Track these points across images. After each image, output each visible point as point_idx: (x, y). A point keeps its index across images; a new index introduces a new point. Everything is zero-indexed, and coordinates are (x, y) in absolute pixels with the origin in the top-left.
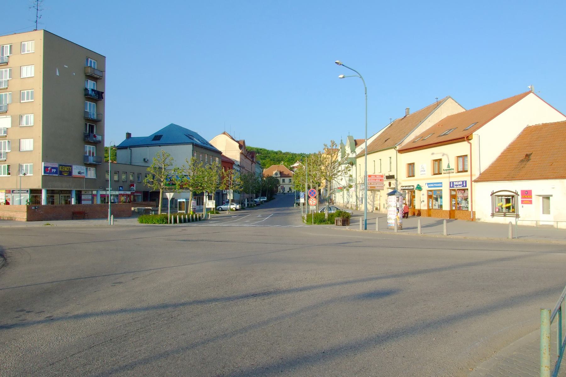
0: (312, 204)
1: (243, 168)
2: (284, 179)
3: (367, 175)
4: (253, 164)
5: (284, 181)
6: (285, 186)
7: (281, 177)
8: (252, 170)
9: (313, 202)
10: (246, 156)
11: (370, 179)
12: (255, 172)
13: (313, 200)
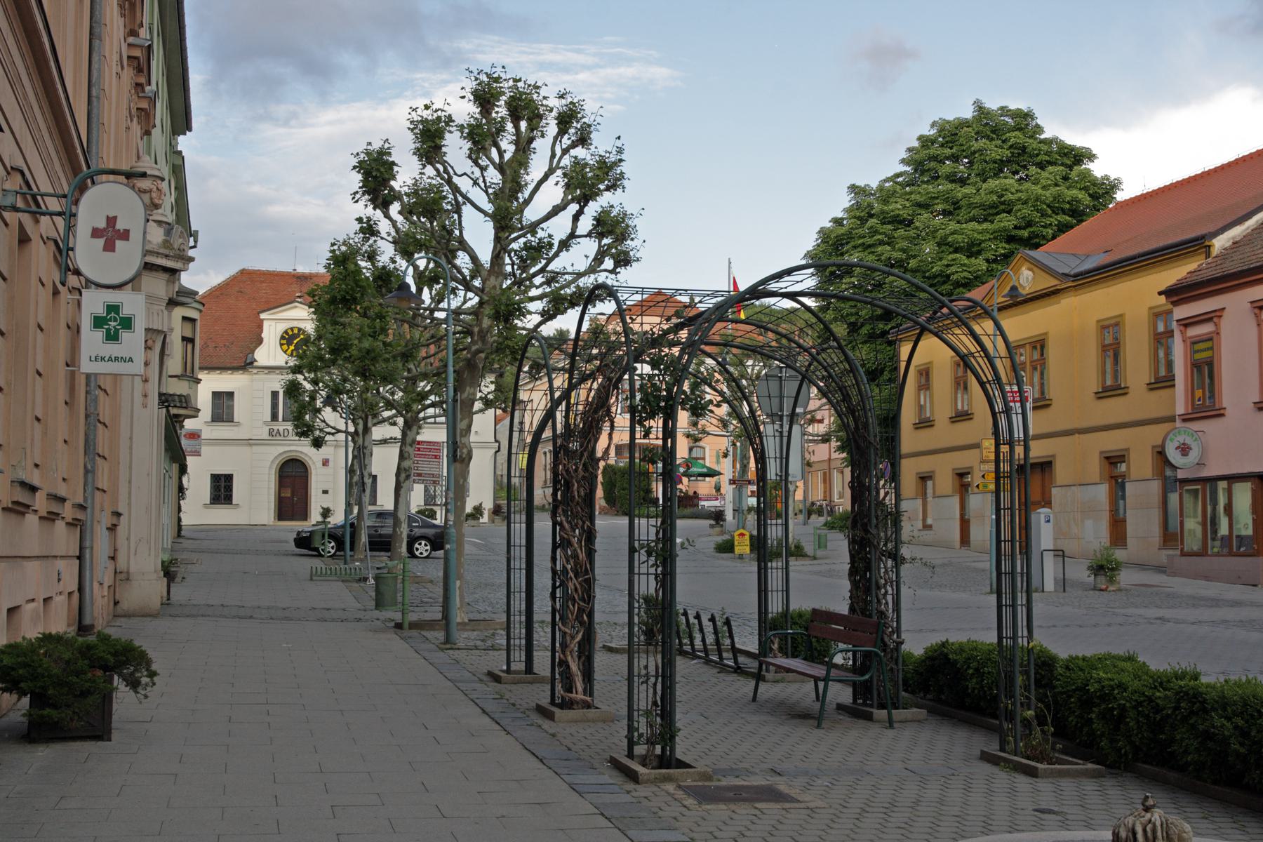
2: (230, 395)
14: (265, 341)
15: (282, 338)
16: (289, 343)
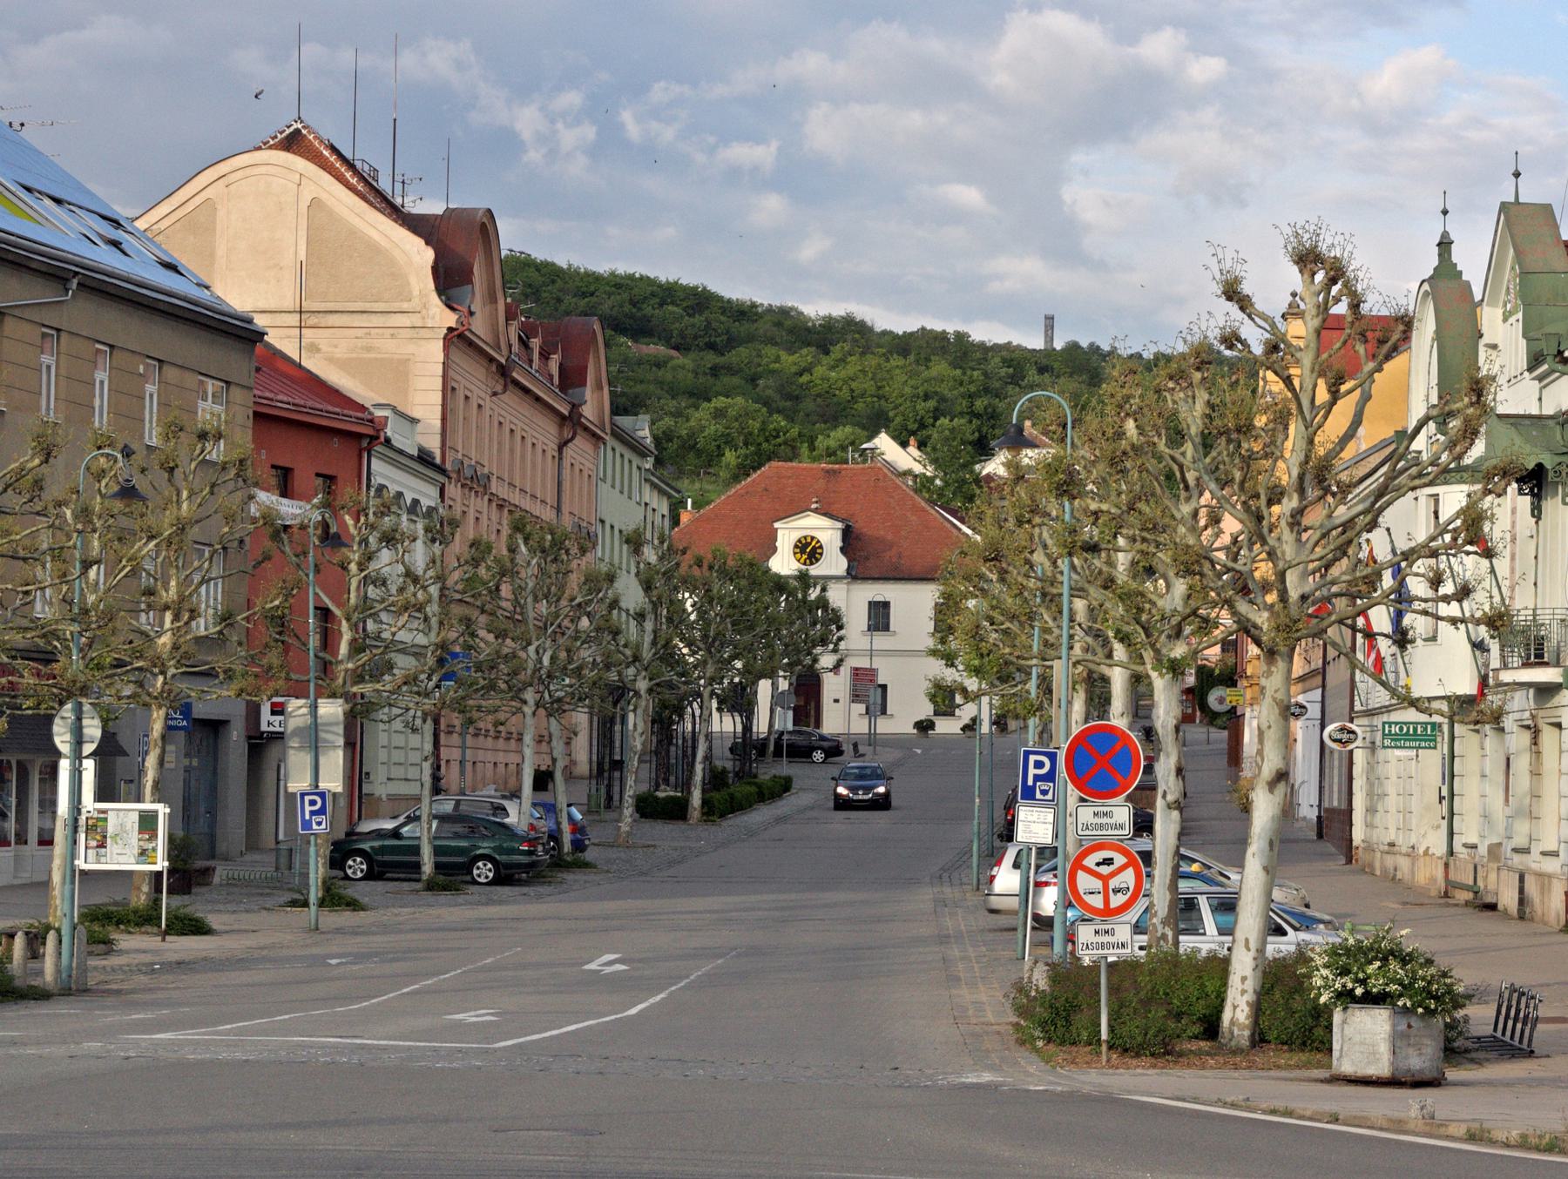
0: (1097, 901)
1: (476, 482)
2: (886, 605)
4: (569, 451)
5: (879, 615)
7: (855, 574)
9: (1113, 883)
10: (503, 371)
14: (779, 550)
15: (796, 546)
16: (803, 552)
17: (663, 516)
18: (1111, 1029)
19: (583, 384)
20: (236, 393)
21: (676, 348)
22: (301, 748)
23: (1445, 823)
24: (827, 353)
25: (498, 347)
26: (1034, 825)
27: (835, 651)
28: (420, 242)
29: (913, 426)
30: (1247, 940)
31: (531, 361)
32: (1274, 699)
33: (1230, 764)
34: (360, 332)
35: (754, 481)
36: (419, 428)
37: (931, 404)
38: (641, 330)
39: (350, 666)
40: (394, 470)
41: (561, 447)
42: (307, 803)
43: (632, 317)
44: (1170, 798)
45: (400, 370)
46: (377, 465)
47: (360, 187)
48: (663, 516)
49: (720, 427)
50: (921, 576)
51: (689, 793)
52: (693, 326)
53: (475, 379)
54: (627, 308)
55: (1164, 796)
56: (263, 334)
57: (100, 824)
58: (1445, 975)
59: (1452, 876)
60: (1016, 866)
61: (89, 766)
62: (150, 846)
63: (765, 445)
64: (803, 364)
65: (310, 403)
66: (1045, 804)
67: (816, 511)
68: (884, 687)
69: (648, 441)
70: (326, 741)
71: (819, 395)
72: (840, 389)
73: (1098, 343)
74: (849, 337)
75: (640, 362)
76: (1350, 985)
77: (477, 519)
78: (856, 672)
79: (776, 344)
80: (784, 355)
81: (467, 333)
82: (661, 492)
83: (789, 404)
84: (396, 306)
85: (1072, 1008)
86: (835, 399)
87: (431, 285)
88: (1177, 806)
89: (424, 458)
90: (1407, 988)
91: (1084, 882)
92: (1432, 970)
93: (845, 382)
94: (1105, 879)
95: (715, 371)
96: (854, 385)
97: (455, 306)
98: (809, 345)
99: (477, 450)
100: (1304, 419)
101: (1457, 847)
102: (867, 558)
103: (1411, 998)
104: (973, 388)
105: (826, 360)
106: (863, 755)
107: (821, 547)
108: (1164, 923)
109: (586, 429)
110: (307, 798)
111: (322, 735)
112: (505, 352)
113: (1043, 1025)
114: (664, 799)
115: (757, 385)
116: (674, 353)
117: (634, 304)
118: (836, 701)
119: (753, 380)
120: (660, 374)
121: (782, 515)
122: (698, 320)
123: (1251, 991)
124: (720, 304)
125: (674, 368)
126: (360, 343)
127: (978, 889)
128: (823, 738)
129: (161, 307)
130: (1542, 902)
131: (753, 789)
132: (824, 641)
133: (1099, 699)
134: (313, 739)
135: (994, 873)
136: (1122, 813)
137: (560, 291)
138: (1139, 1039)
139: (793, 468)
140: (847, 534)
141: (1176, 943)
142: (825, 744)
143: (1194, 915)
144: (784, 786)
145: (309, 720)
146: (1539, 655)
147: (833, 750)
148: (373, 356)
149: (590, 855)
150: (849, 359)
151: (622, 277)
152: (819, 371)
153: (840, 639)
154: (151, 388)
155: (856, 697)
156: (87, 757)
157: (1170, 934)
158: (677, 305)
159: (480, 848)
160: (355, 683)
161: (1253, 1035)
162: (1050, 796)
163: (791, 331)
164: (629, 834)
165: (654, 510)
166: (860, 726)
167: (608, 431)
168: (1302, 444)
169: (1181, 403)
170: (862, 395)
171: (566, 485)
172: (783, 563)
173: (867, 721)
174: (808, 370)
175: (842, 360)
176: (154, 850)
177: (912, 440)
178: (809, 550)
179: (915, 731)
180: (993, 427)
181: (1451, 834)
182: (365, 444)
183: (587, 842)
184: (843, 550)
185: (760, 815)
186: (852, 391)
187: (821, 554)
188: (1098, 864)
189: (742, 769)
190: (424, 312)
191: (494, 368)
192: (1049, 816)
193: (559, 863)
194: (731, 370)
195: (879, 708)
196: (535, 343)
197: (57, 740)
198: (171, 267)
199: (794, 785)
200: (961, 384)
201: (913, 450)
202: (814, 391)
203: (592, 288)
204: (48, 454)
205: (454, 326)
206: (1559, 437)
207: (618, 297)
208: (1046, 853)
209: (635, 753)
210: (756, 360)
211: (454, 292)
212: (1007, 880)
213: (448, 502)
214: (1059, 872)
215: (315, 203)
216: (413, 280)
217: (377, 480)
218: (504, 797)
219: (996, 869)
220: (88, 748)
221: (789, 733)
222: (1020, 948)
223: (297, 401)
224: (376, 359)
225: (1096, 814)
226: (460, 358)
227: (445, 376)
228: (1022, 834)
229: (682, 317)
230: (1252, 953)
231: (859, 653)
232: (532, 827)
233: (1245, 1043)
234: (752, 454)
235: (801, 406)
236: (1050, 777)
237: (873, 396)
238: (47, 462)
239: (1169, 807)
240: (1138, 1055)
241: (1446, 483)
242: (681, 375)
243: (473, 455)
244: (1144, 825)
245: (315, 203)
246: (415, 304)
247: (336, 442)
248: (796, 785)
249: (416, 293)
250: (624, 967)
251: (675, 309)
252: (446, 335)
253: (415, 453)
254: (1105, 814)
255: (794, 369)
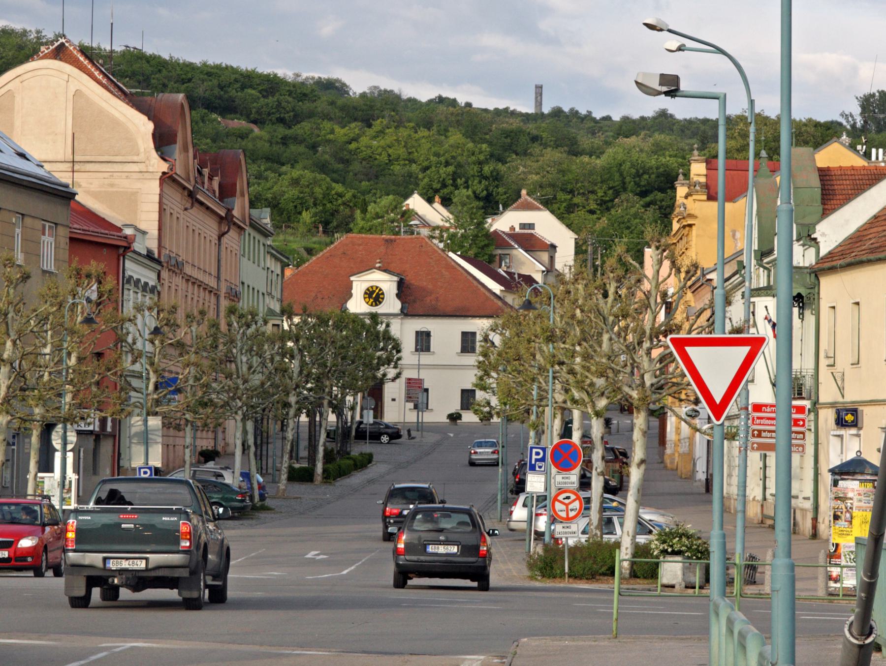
0: (564, 515)
1: (177, 267)
2: (428, 334)
3: (750, 402)
4: (225, 240)
5: (423, 341)
6: (429, 379)
7: (406, 313)
8: (218, 278)
9: (570, 507)
10: (191, 195)
11: (758, 418)
12: (239, 289)
13: (568, 498)
14: (354, 295)
16: (370, 297)
17: (278, 275)
18: (570, 568)
19: (175, 142)
20: (60, 229)
21: (255, 122)
22: (139, 443)
23: (761, 482)
24: (370, 126)
25: (188, 180)
26: (535, 483)
27: (395, 367)
28: (144, 118)
29: (437, 186)
30: (628, 532)
31: (203, 183)
32: (640, 429)
33: (660, 444)
34: (106, 175)
35: (335, 247)
36: (147, 236)
37: (451, 169)
38: (228, 109)
39: (155, 396)
40: (144, 269)
41: (220, 237)
42: (142, 473)
43: (220, 98)
44: (599, 470)
45: (132, 199)
46: (128, 264)
47: (104, 81)
48: (278, 275)
49: (297, 193)
50: (451, 314)
51: (314, 465)
52: (267, 104)
53: (177, 202)
54: (217, 91)
55: (596, 470)
56: (75, 194)
57: (40, 484)
58: (705, 543)
59: (765, 512)
60: (525, 505)
61: (70, 456)
62: (68, 496)
63: (329, 205)
64: (352, 135)
65: (91, 229)
66: (540, 473)
67: (379, 269)
68: (427, 390)
69: (269, 226)
70: (151, 439)
71: (364, 159)
72: (380, 154)
73: (577, 108)
74: (386, 113)
75: (228, 135)
76: (666, 548)
77: (170, 287)
78: (409, 380)
79: (330, 119)
80: (337, 129)
81: (174, 175)
82: (277, 259)
83: (341, 166)
84: (129, 159)
85: (553, 561)
86: (376, 162)
87: (152, 145)
88: (602, 474)
89: (149, 256)
90: (689, 549)
91: (558, 506)
92: (700, 541)
93: (384, 148)
94: (567, 505)
95: (285, 141)
96: (390, 151)
97: (167, 158)
98: (355, 120)
99: (178, 248)
100: (652, 310)
101: (768, 496)
102: (414, 301)
103: (691, 552)
104: (482, 157)
105: (370, 132)
106: (413, 438)
107: (383, 294)
108: (596, 528)
109: (235, 224)
110: (142, 470)
111: (150, 436)
112: (193, 182)
113: (541, 570)
114: (298, 469)
115: (317, 151)
116: (252, 126)
117: (221, 88)
118: (394, 400)
119: (314, 147)
120: (243, 143)
121: (356, 271)
122: (271, 100)
123: (630, 553)
124: (287, 88)
125: (254, 139)
126: (107, 181)
127: (501, 521)
128: (387, 426)
129: (25, 183)
130: (803, 524)
131: (351, 462)
132: (388, 361)
133: (567, 432)
134: (145, 439)
135: (512, 509)
136: (574, 477)
137: (165, 78)
138: (581, 572)
139: (362, 238)
140: (401, 284)
141: (602, 538)
142: (390, 431)
143: (611, 526)
144: (366, 461)
145: (143, 428)
146: (800, 394)
147: (395, 435)
148: (115, 190)
149: (268, 502)
150: (387, 131)
151: (212, 68)
152: (364, 140)
153: (399, 359)
154: (18, 231)
155: (409, 398)
156: (69, 451)
157: (599, 533)
158: (254, 89)
159: (213, 498)
160: (157, 406)
161: (630, 573)
162: (543, 469)
163: (343, 108)
164: (284, 490)
165: (272, 272)
166: (412, 417)
167: (248, 223)
168: (651, 318)
169: (600, 300)
170: (397, 159)
171: (223, 263)
172: (357, 305)
173: (416, 413)
174: (355, 139)
175: (382, 132)
176: (70, 498)
177: (437, 199)
178: (374, 296)
179: (448, 421)
180: (497, 187)
181: (765, 488)
182: (121, 251)
183: (266, 495)
184: (398, 296)
185: (357, 479)
186: (389, 155)
187: (383, 299)
188: (564, 499)
189: (341, 449)
190: (147, 162)
191: (186, 193)
192: (542, 478)
193: (254, 508)
194: (296, 140)
195: (425, 405)
196: (206, 171)
197: (54, 443)
198: (22, 156)
199: (374, 459)
200: (473, 154)
201: (437, 205)
202: (361, 156)
203: (190, 76)
204: (61, 306)
205: (166, 170)
206: (808, 280)
207: (210, 83)
208: (542, 498)
209: (288, 441)
210: (316, 132)
211: (166, 149)
212: (519, 513)
213: (162, 281)
214: (547, 508)
215: (78, 94)
216: (140, 142)
217: (128, 273)
218: (222, 469)
219: (513, 507)
220: (69, 447)
221: (371, 425)
222: (527, 547)
223: (85, 228)
224: (117, 192)
225: (563, 478)
226: (170, 191)
227: (161, 203)
228: (529, 488)
229: (259, 98)
230: (630, 538)
231: (411, 367)
232: (240, 487)
233: (627, 576)
234: (321, 212)
235: (351, 168)
236: (543, 459)
237: (404, 160)
238: (60, 309)
239: (598, 474)
240: (581, 579)
241: (759, 296)
242: (259, 144)
243: (174, 251)
244: (585, 483)
245: (78, 94)
246: (142, 157)
247: (105, 251)
248: (375, 458)
249: (142, 150)
250: (325, 557)
251: (253, 92)
252: (161, 177)
253: (144, 252)
254: (567, 478)
255: (345, 139)
